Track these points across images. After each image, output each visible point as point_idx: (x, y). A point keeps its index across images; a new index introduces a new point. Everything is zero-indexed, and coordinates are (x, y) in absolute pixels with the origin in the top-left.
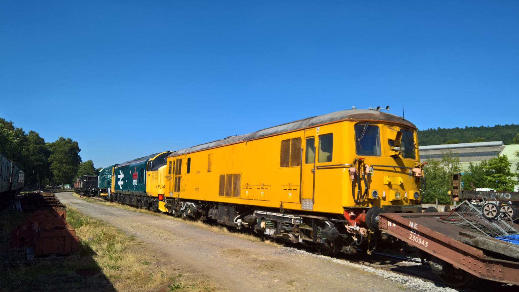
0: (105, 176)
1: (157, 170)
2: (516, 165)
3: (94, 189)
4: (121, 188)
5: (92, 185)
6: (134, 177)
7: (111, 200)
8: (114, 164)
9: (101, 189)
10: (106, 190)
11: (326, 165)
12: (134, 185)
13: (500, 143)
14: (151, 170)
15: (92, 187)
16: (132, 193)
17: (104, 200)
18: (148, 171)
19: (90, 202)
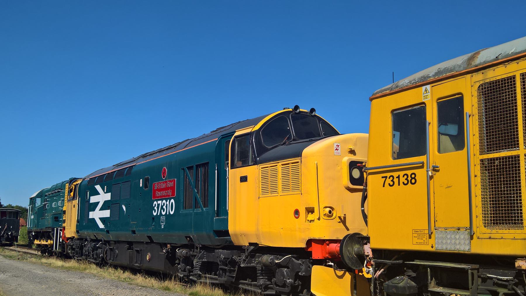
0: (46, 204)
1: (299, 154)
2: (340, 222)
3: (12, 233)
4: (101, 226)
5: (8, 226)
6: (158, 194)
7: (64, 256)
8: (68, 179)
9: (34, 232)
10: (50, 232)
11: (445, 265)
12: (158, 217)
13: (261, 254)
14: (255, 163)
15: (8, 229)
16: (149, 237)
17: (39, 253)
18: (232, 168)
19: (11, 257)
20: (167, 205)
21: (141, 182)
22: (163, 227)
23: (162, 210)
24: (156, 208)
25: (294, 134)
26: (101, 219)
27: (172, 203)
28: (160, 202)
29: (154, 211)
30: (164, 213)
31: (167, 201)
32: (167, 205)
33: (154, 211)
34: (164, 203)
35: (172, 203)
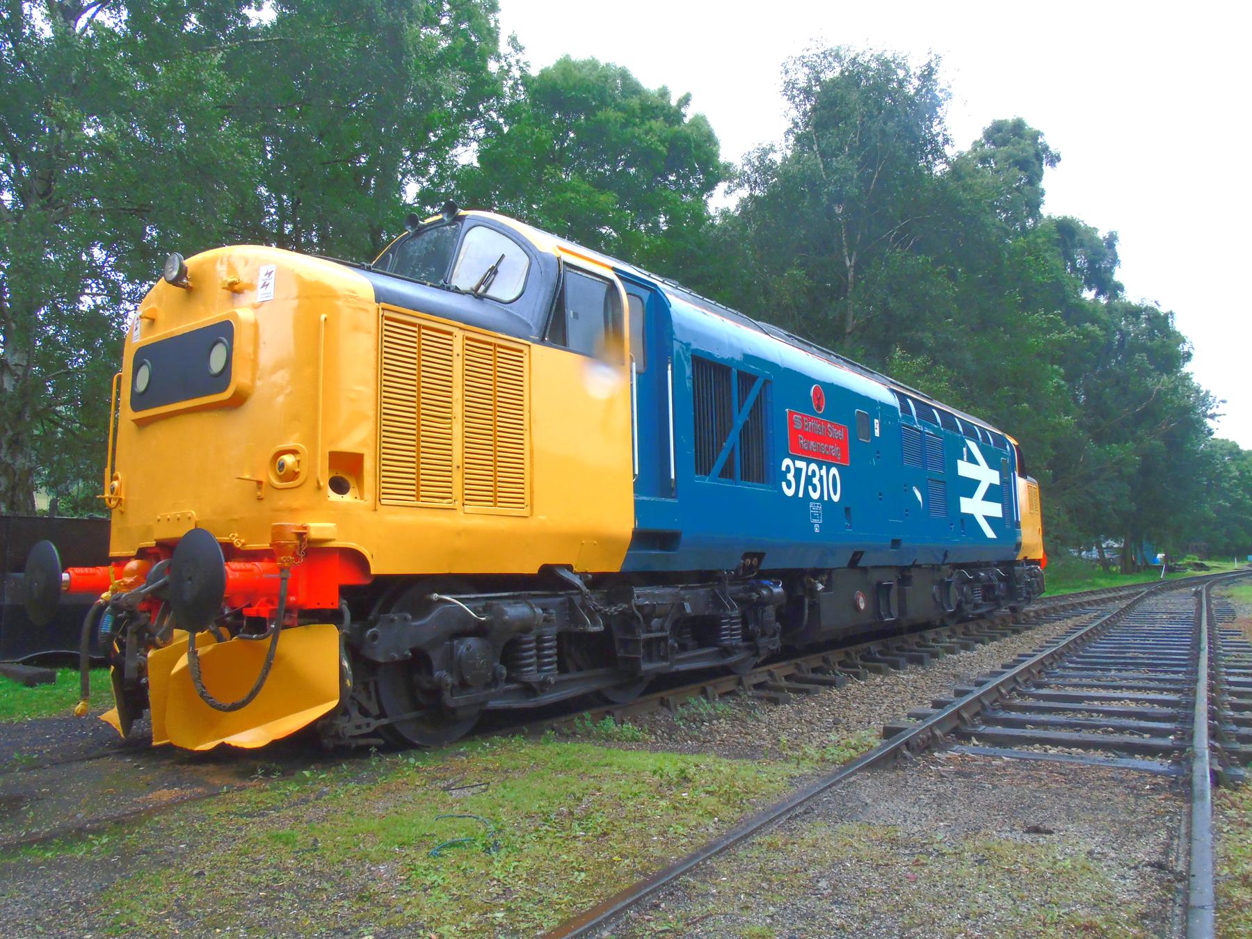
4: (990, 533)
18: (381, 296)
20: (821, 477)
21: (877, 426)
22: (817, 530)
23: (810, 488)
24: (790, 476)
25: (506, 594)
26: (986, 517)
27: (834, 475)
28: (801, 464)
29: (784, 484)
30: (815, 496)
31: (820, 468)
32: (821, 477)
33: (784, 484)
34: (814, 472)
35: (834, 475)
